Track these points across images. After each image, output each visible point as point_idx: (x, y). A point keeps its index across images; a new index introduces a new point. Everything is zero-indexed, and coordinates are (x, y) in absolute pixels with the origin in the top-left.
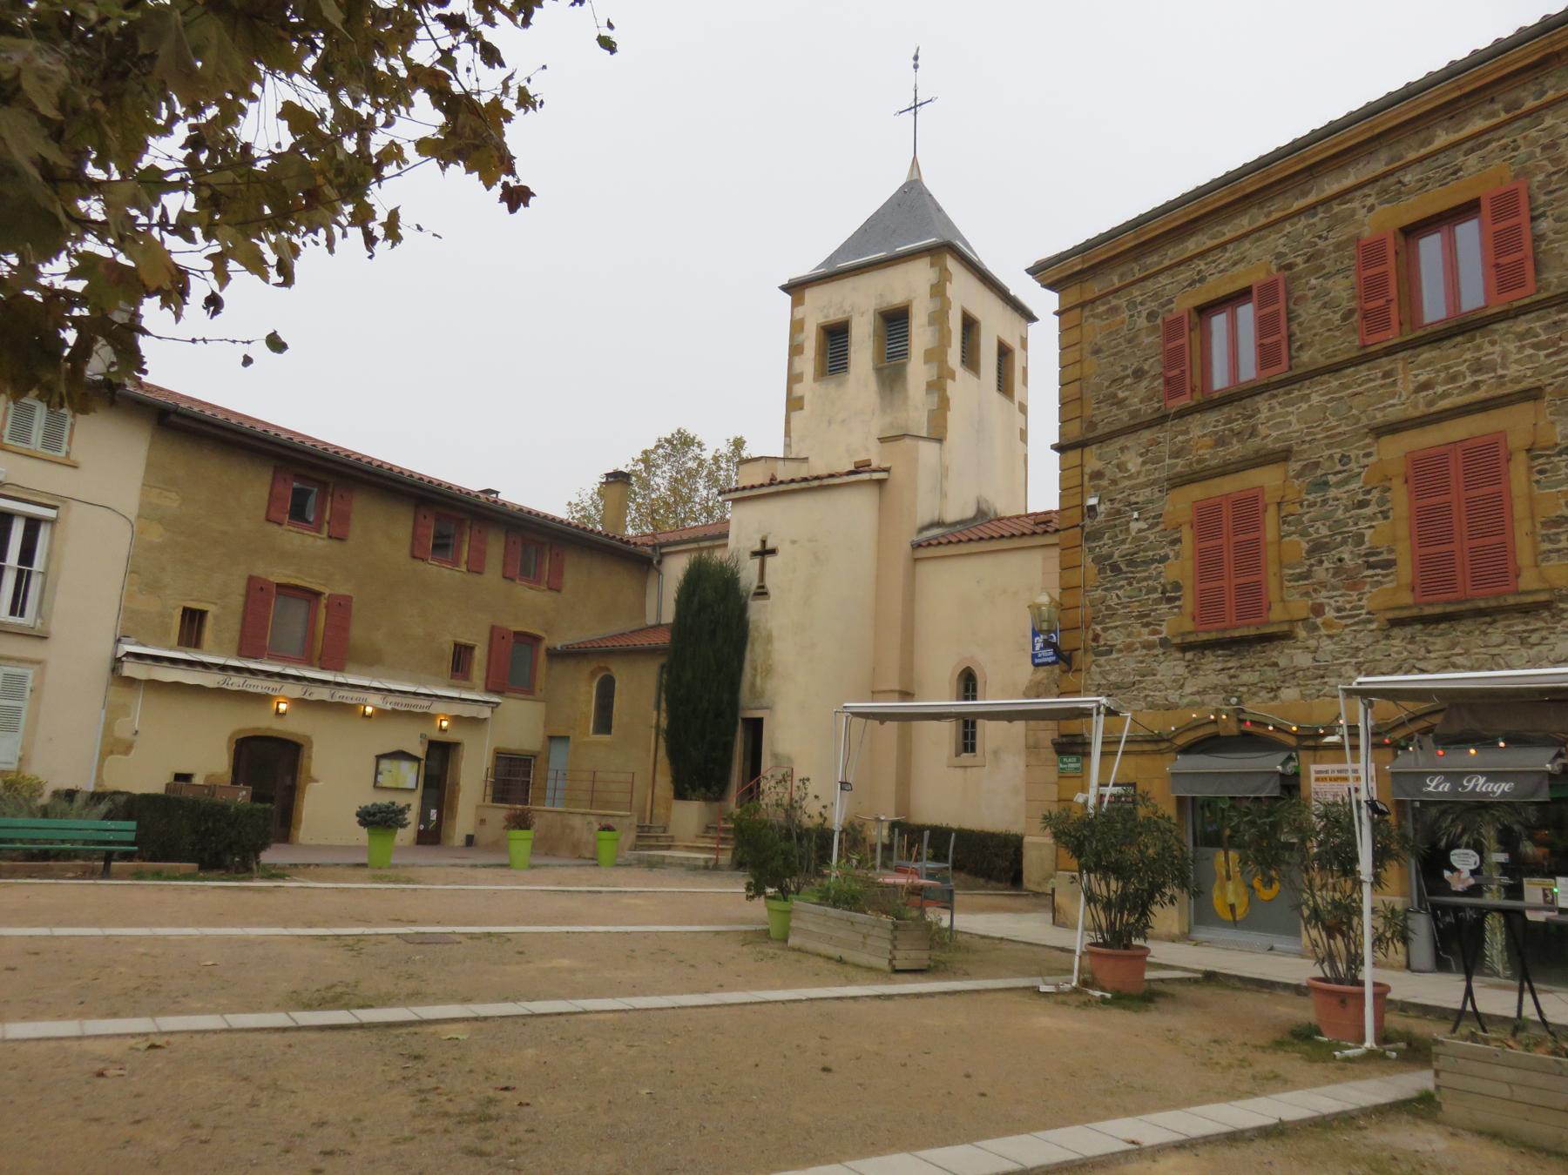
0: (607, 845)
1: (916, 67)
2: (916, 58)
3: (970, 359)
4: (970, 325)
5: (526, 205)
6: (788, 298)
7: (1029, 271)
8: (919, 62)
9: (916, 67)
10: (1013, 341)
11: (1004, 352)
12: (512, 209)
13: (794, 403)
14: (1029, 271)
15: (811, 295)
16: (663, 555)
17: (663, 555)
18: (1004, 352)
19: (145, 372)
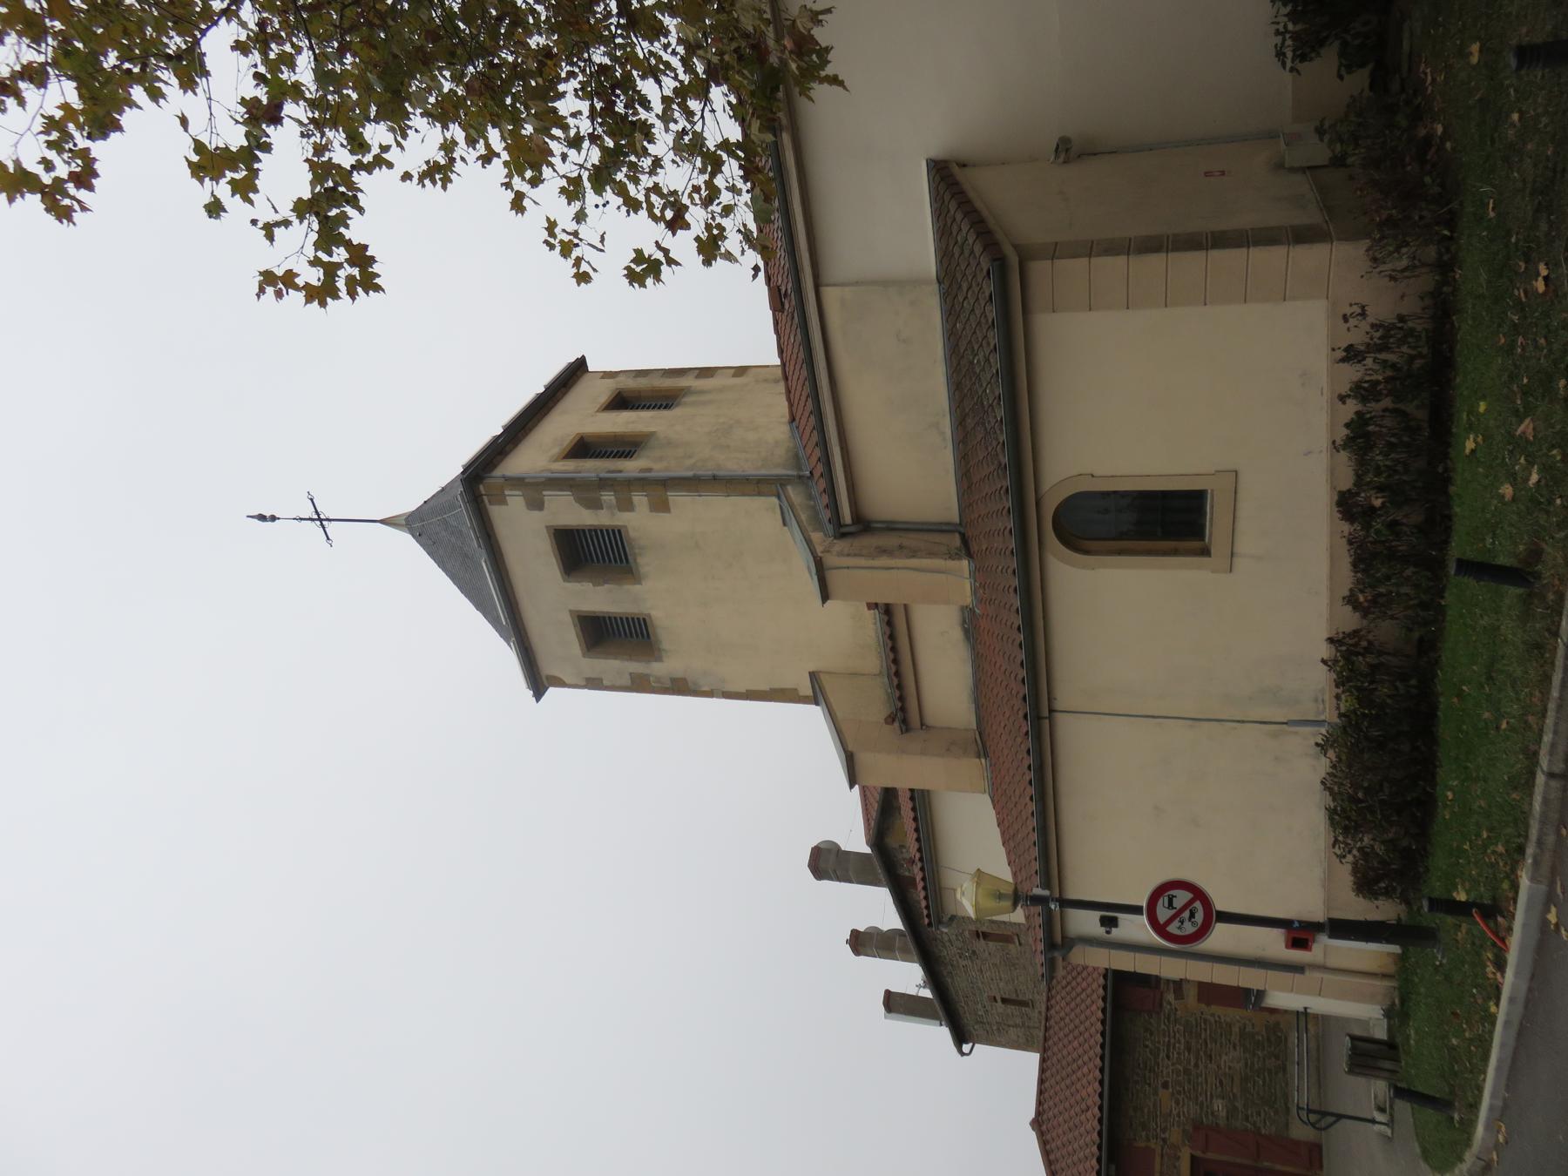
0: (1453, 248)
1: (273, 518)
2: (262, 518)
3: (625, 447)
4: (583, 448)
5: (366, 247)
6: (552, 692)
7: (538, 700)
8: (268, 515)
9: (273, 518)
10: (604, 392)
11: (621, 402)
12: (378, 288)
13: (679, 686)
14: (538, 700)
15: (547, 668)
16: (858, 518)
17: (858, 518)
18: (621, 402)
19: (561, 533)
